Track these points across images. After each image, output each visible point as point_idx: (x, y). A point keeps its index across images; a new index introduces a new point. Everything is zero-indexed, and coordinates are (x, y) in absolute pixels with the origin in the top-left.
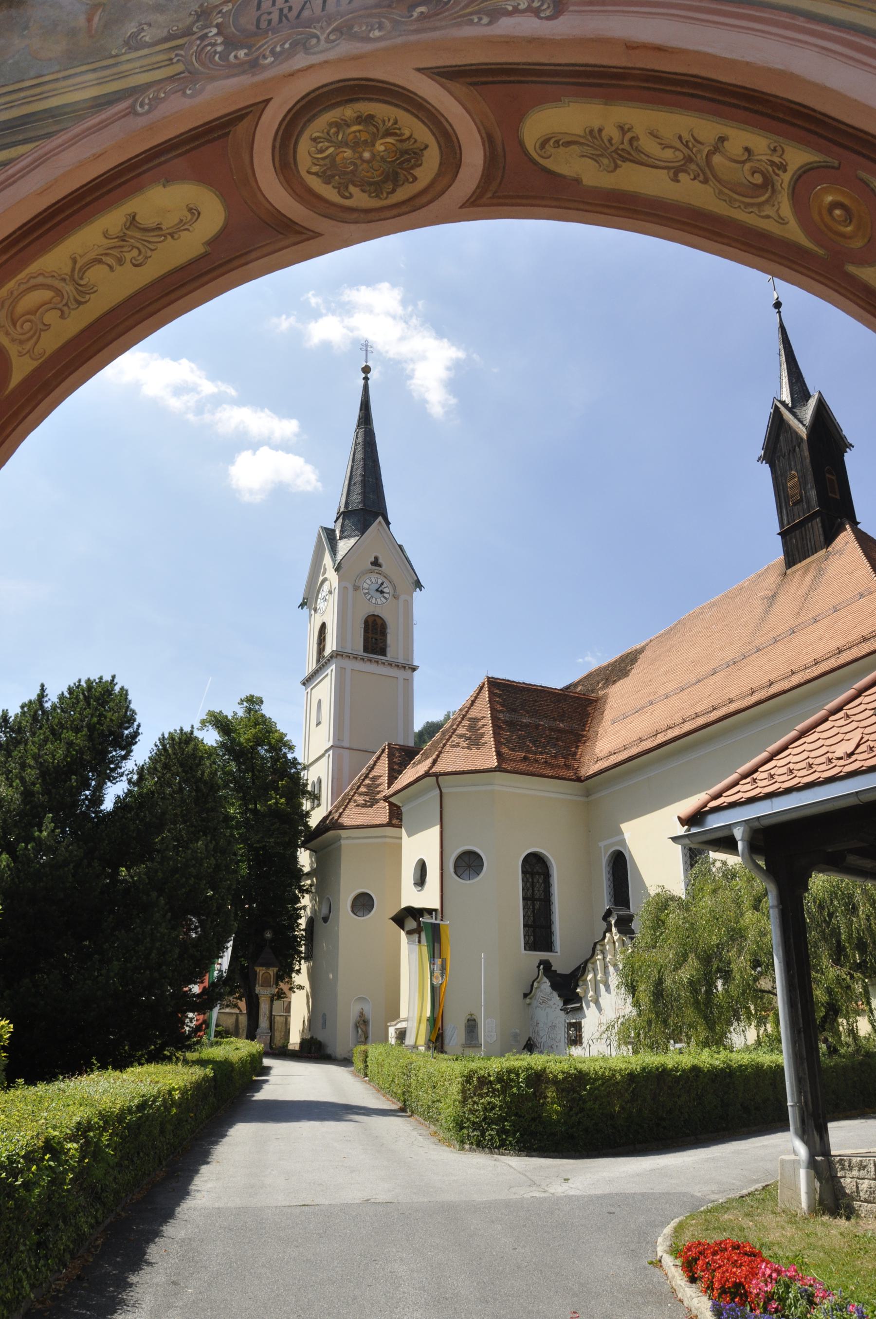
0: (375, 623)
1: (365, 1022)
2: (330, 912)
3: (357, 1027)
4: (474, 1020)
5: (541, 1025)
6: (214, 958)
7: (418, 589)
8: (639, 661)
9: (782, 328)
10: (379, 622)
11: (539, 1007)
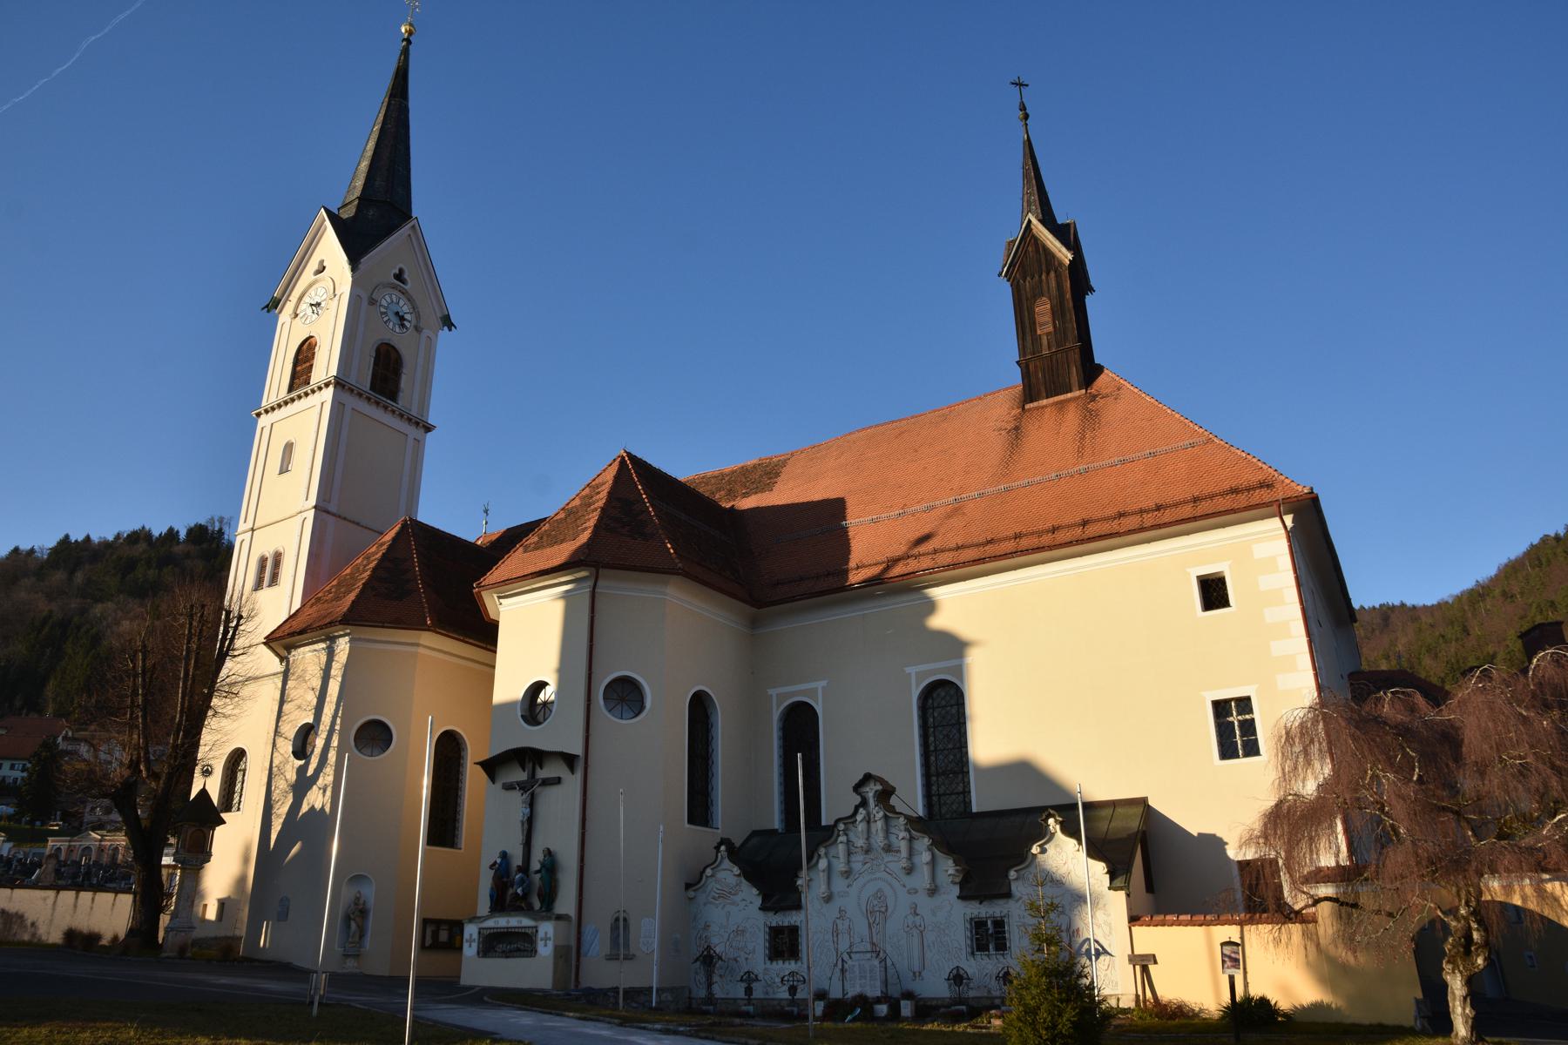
2: (274, 740)
6: (1488, 964)
7: (446, 328)
8: (783, 476)
9: (1029, 144)
11: (710, 903)
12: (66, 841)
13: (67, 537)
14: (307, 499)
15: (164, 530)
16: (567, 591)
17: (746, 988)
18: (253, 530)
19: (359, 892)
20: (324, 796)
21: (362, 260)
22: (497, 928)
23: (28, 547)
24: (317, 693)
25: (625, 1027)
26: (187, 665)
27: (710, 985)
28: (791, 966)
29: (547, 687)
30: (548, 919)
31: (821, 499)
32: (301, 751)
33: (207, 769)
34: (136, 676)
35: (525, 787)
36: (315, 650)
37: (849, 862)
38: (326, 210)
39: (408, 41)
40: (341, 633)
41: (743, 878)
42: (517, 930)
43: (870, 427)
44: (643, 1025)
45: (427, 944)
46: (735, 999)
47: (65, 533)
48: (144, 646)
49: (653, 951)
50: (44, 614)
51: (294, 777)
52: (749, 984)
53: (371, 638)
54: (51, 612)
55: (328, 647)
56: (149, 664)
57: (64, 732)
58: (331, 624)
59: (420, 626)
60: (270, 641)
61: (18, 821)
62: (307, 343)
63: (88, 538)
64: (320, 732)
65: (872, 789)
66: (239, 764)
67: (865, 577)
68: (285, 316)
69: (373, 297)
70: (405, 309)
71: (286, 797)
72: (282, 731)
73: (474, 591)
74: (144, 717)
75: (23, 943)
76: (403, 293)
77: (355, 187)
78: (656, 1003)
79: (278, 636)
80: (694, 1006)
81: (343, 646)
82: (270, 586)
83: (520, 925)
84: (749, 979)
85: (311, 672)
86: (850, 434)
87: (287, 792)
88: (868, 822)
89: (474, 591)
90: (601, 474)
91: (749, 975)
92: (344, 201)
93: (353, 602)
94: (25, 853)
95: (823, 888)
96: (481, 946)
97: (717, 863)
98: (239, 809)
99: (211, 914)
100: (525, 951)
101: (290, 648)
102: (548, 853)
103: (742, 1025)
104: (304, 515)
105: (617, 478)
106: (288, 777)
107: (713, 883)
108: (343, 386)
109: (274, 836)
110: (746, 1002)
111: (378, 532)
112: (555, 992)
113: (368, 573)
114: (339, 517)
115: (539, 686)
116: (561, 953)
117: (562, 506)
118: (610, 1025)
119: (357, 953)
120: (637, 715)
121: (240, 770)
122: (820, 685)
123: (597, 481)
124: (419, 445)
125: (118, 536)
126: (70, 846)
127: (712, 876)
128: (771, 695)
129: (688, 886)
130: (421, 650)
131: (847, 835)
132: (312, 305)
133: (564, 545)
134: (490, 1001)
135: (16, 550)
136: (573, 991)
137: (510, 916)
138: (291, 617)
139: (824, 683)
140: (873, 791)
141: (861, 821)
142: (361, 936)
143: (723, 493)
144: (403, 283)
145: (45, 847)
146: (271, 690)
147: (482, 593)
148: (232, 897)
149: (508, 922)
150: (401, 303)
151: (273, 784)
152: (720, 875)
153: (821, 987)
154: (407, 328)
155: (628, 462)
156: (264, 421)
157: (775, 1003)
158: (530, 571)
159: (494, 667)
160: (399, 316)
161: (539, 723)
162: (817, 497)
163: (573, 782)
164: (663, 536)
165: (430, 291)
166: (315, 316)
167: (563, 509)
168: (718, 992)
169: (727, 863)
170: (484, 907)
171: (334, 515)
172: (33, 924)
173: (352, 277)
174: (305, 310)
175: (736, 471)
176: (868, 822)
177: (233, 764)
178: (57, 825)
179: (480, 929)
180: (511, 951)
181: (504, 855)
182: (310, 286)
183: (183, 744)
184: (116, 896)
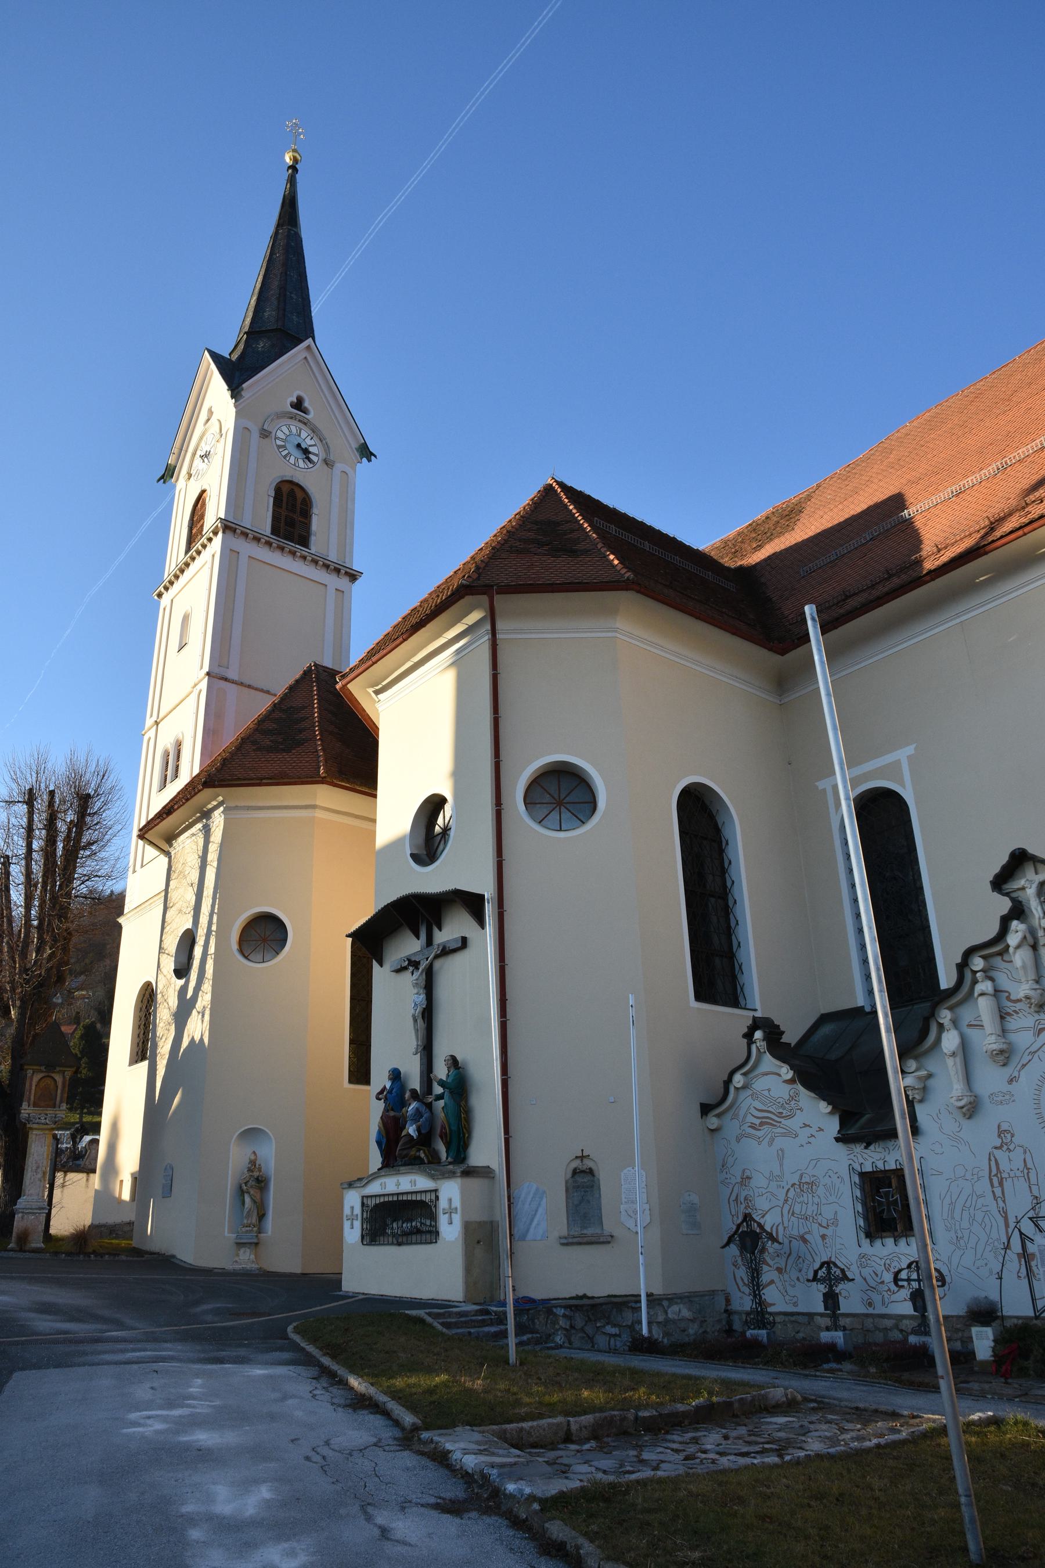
0: (292, 494)
1: (261, 1183)
3: (241, 1192)
4: (591, 1172)
5: (759, 1181)
7: (364, 460)
10: (299, 495)
11: (749, 1136)
16: (458, 652)
18: (157, 723)
19: (254, 1153)
20: (203, 1021)
22: (384, 1195)
24: (195, 890)
28: (905, 1251)
37: (1004, 1032)
46: (811, 1315)
59: (311, 778)
65: (1031, 882)
69: (265, 427)
71: (169, 1030)
72: (165, 947)
76: (305, 424)
85: (190, 864)
87: (169, 1023)
88: (1035, 947)
91: (829, 1269)
95: (958, 1088)
101: (170, 838)
102: (454, 1062)
106: (171, 1004)
107: (749, 1100)
108: (234, 531)
114: (242, 684)
119: (255, 1241)
122: (903, 754)
127: (745, 1087)
128: (824, 790)
129: (706, 1109)
130: (319, 814)
131: (992, 979)
137: (398, 1173)
139: (910, 750)
140: (1034, 886)
141: (1018, 947)
142: (262, 1216)
144: (305, 413)
147: (349, 686)
149: (398, 1184)
150: (304, 434)
152: (760, 1084)
153: (983, 1295)
157: (889, 1323)
168: (776, 1299)
169: (769, 1062)
171: (233, 682)
173: (236, 407)
176: (1035, 947)
179: (363, 1197)
180: (406, 1234)
184: (65, 1176)
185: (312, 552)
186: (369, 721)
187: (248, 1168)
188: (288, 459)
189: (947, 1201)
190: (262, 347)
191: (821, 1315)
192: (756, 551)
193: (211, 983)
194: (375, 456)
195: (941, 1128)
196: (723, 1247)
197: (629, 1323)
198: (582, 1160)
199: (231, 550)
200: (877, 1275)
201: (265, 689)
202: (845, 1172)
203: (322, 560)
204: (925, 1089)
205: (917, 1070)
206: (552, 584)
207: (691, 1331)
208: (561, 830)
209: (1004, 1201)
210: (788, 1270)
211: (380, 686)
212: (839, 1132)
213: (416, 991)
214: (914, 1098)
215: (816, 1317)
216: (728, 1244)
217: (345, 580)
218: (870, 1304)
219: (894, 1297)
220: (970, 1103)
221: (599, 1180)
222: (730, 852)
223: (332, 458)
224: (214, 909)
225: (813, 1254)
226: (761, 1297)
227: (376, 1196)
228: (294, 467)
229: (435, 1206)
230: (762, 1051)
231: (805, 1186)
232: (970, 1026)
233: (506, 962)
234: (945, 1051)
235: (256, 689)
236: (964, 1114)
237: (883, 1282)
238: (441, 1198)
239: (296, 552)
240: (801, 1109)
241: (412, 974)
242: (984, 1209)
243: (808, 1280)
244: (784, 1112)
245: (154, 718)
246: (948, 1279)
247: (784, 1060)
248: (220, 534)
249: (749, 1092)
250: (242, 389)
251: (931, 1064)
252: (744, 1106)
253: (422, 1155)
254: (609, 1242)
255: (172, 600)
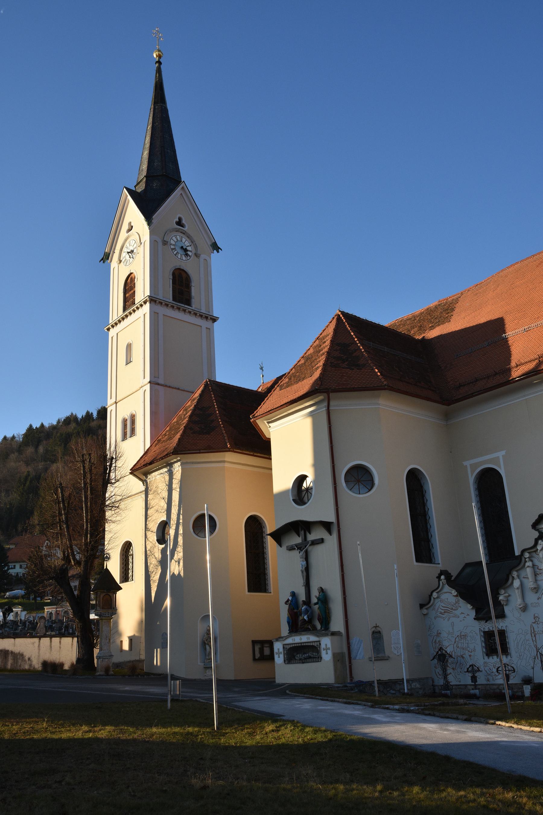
4: (379, 632)
5: (444, 635)
7: (215, 251)
8: (456, 310)
11: (440, 617)
12: (54, 608)
13: (31, 426)
14: (144, 378)
15: (84, 414)
16: (311, 412)
17: (471, 677)
18: (116, 403)
20: (179, 566)
21: (153, 217)
22: (294, 644)
23: (11, 435)
24: (166, 501)
25: (376, 708)
26: (86, 492)
27: (445, 676)
29: (307, 479)
30: (326, 635)
31: (485, 321)
32: (162, 539)
33: (107, 556)
34: (59, 503)
35: (301, 547)
36: (162, 474)
37: (536, 580)
38: (127, 189)
39: (159, 62)
40: (175, 460)
41: (460, 598)
42: (307, 644)
43: (517, 263)
44: (387, 706)
45: (257, 658)
46: (466, 686)
47: (30, 424)
48: (61, 484)
49: (401, 653)
50: (25, 474)
51: (160, 556)
52: (474, 674)
53: (195, 461)
54: (28, 472)
55: (168, 471)
56: (66, 494)
57: (46, 544)
58: (167, 455)
59: (224, 449)
60: (134, 471)
61: (29, 598)
62: (130, 278)
63: (42, 425)
64: (171, 525)
66: (129, 552)
67: (523, 372)
68: (114, 263)
69: (165, 239)
70: (187, 243)
71: (157, 569)
72: (149, 528)
73: (251, 421)
74: (68, 528)
75: (26, 671)
76: (184, 234)
77: (142, 169)
78: (408, 689)
79: (138, 467)
80: (437, 691)
81: (177, 468)
82: (131, 437)
83: (308, 641)
84: (473, 670)
85: (161, 488)
86: (502, 271)
87: (157, 566)
89: (251, 421)
90: (325, 329)
91: (473, 667)
92: (137, 181)
93: (179, 439)
94: (33, 617)
95: (519, 601)
96: (286, 656)
97: (440, 588)
98: (133, 580)
99: (126, 646)
100: (314, 658)
101: (146, 474)
102: (322, 590)
103: (465, 704)
104: (144, 388)
105: (336, 330)
106: (157, 556)
108: (155, 301)
109: (153, 595)
110: (473, 687)
111: (191, 392)
112: (337, 685)
113: (187, 419)
114: (166, 386)
115: (302, 478)
116: (338, 658)
117: (302, 355)
118: (365, 707)
120: (370, 490)
121: (130, 555)
122: (501, 454)
123: (323, 335)
124: (210, 331)
125: (59, 421)
126: (57, 611)
127: (438, 598)
129: (422, 606)
130: (227, 465)
131: (532, 561)
132: (128, 253)
133: (305, 381)
134: (290, 693)
135: (5, 438)
136: (349, 683)
137: (301, 635)
138: (146, 453)
139: (503, 453)
143: (416, 329)
144: (183, 227)
145: (44, 612)
146: (140, 502)
148: (136, 634)
149: (301, 639)
150: (184, 240)
151: (149, 561)
152: (444, 597)
153: (527, 675)
154: (190, 256)
155: (343, 318)
156: (113, 332)
157: (495, 687)
158: (284, 402)
159: (271, 469)
160: (184, 249)
161: (304, 503)
162: (483, 320)
163: (331, 541)
164: (372, 365)
165: (199, 225)
166: (131, 259)
167: (303, 357)
168: (452, 680)
169: (447, 588)
170: (285, 629)
172: (29, 659)
174: (125, 257)
175: (423, 312)
177: (126, 552)
178: (49, 599)
179: (284, 645)
180: (305, 659)
181: (293, 594)
182: (126, 240)
183: (90, 542)
185: (193, 308)
186: (260, 431)
187: (207, 633)
188: (173, 251)
189: (516, 642)
190: (156, 186)
191: (470, 685)
192: (431, 330)
193: (182, 547)
194: (221, 250)
195: (513, 615)
196: (432, 660)
197: (398, 689)
198: (376, 628)
199: (154, 312)
200: (491, 670)
201: (177, 387)
202: (478, 632)
203: (199, 313)
204: (507, 601)
205: (505, 593)
206: (353, 388)
207: (420, 693)
208: (360, 494)
209: (536, 642)
210: (457, 668)
211: (270, 420)
212: (475, 616)
213: (302, 560)
214: (503, 604)
215: (468, 686)
216: (433, 659)
217: (210, 322)
218: (488, 680)
219: (497, 678)
220: (524, 606)
221: (383, 635)
222: (427, 496)
223: (199, 253)
224: (180, 512)
225: (466, 662)
226: (447, 678)
227: (290, 644)
228: (180, 260)
229: (319, 647)
230: (444, 583)
231: (463, 637)
232: (524, 578)
233: (342, 549)
234: (515, 587)
235: (173, 388)
236: (522, 610)
237: (493, 672)
238: (322, 644)
239: (186, 310)
240: (460, 607)
241: (300, 553)
242: (529, 645)
243: (465, 672)
244: (454, 608)
245: (113, 400)
246: (516, 670)
247: (453, 587)
248: (148, 304)
249: (439, 600)
250: (153, 219)
251: (510, 591)
252: (437, 605)
253: (310, 627)
254: (388, 659)
255: (117, 334)
